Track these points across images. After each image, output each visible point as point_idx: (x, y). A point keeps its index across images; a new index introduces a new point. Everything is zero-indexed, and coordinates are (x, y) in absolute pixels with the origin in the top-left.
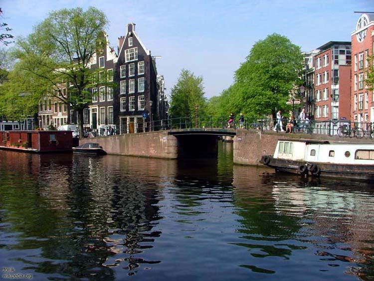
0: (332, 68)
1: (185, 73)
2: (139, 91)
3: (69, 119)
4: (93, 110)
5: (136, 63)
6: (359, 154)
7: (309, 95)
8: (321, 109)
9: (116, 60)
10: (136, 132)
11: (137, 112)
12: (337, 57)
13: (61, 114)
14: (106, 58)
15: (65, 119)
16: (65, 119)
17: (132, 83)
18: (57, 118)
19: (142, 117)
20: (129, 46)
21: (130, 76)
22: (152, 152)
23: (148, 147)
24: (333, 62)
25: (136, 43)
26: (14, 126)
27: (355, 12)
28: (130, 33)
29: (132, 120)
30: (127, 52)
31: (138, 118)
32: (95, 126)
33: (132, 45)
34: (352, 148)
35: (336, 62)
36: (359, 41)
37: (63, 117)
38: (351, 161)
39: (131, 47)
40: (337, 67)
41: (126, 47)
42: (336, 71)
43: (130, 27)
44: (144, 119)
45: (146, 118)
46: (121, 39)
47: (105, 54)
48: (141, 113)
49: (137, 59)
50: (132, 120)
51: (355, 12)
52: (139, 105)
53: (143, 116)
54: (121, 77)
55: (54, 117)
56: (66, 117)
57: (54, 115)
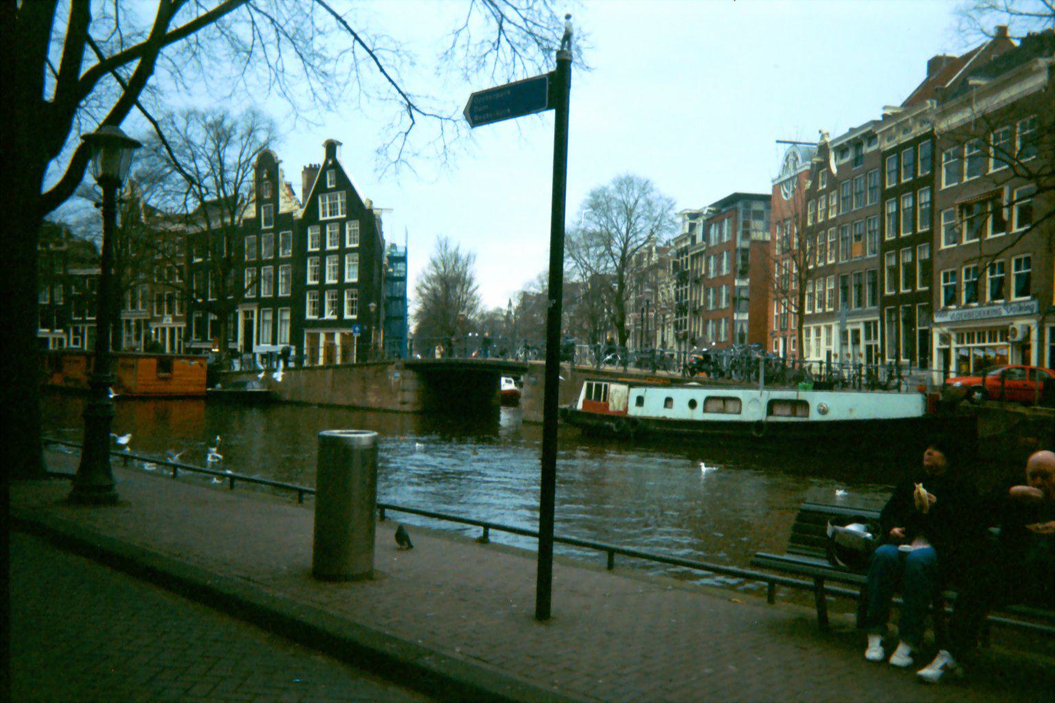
0: (738, 245)
1: (443, 245)
2: (347, 280)
3: (189, 328)
4: (246, 314)
5: (342, 223)
6: (712, 405)
7: (711, 297)
8: (714, 326)
9: (299, 214)
10: (988, 298)
11: (340, 323)
12: (746, 224)
13: (170, 319)
14: (277, 207)
15: (180, 329)
16: (180, 329)
17: (330, 263)
18: (159, 326)
19: (352, 331)
20: (329, 186)
21: (329, 247)
22: (372, 400)
23: (364, 390)
24: (739, 234)
25: (343, 183)
26: (54, 340)
27: (778, 142)
28: (330, 162)
29: (330, 336)
30: (324, 200)
31: (343, 335)
32: (248, 347)
33: (333, 186)
34: (700, 395)
35: (746, 235)
36: (785, 198)
37: (177, 325)
38: (698, 415)
39: (332, 190)
40: (746, 244)
41: (321, 188)
42: (744, 250)
43: (331, 147)
44: (356, 335)
45: (359, 335)
46: (310, 171)
47: (275, 199)
48: (349, 323)
49: (344, 216)
50: (330, 336)
51: (778, 142)
52: (346, 307)
53: (355, 331)
54: (310, 249)
55: (154, 326)
56: (183, 325)
57: (153, 319)
